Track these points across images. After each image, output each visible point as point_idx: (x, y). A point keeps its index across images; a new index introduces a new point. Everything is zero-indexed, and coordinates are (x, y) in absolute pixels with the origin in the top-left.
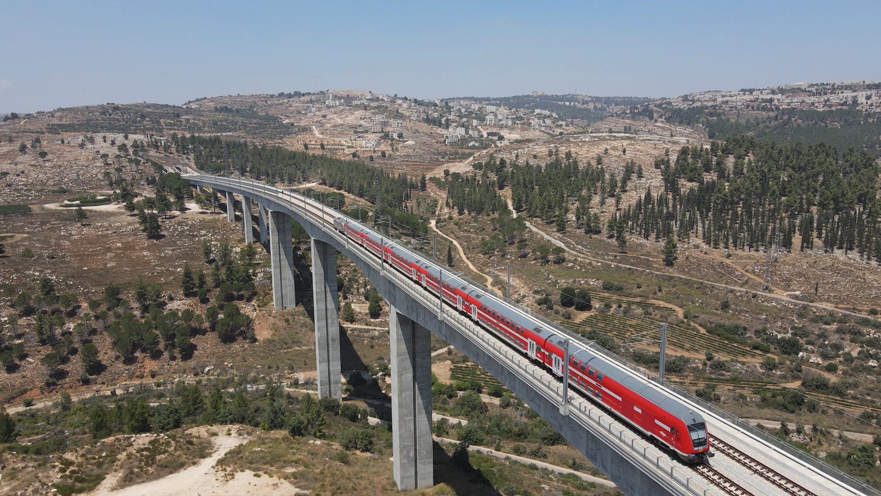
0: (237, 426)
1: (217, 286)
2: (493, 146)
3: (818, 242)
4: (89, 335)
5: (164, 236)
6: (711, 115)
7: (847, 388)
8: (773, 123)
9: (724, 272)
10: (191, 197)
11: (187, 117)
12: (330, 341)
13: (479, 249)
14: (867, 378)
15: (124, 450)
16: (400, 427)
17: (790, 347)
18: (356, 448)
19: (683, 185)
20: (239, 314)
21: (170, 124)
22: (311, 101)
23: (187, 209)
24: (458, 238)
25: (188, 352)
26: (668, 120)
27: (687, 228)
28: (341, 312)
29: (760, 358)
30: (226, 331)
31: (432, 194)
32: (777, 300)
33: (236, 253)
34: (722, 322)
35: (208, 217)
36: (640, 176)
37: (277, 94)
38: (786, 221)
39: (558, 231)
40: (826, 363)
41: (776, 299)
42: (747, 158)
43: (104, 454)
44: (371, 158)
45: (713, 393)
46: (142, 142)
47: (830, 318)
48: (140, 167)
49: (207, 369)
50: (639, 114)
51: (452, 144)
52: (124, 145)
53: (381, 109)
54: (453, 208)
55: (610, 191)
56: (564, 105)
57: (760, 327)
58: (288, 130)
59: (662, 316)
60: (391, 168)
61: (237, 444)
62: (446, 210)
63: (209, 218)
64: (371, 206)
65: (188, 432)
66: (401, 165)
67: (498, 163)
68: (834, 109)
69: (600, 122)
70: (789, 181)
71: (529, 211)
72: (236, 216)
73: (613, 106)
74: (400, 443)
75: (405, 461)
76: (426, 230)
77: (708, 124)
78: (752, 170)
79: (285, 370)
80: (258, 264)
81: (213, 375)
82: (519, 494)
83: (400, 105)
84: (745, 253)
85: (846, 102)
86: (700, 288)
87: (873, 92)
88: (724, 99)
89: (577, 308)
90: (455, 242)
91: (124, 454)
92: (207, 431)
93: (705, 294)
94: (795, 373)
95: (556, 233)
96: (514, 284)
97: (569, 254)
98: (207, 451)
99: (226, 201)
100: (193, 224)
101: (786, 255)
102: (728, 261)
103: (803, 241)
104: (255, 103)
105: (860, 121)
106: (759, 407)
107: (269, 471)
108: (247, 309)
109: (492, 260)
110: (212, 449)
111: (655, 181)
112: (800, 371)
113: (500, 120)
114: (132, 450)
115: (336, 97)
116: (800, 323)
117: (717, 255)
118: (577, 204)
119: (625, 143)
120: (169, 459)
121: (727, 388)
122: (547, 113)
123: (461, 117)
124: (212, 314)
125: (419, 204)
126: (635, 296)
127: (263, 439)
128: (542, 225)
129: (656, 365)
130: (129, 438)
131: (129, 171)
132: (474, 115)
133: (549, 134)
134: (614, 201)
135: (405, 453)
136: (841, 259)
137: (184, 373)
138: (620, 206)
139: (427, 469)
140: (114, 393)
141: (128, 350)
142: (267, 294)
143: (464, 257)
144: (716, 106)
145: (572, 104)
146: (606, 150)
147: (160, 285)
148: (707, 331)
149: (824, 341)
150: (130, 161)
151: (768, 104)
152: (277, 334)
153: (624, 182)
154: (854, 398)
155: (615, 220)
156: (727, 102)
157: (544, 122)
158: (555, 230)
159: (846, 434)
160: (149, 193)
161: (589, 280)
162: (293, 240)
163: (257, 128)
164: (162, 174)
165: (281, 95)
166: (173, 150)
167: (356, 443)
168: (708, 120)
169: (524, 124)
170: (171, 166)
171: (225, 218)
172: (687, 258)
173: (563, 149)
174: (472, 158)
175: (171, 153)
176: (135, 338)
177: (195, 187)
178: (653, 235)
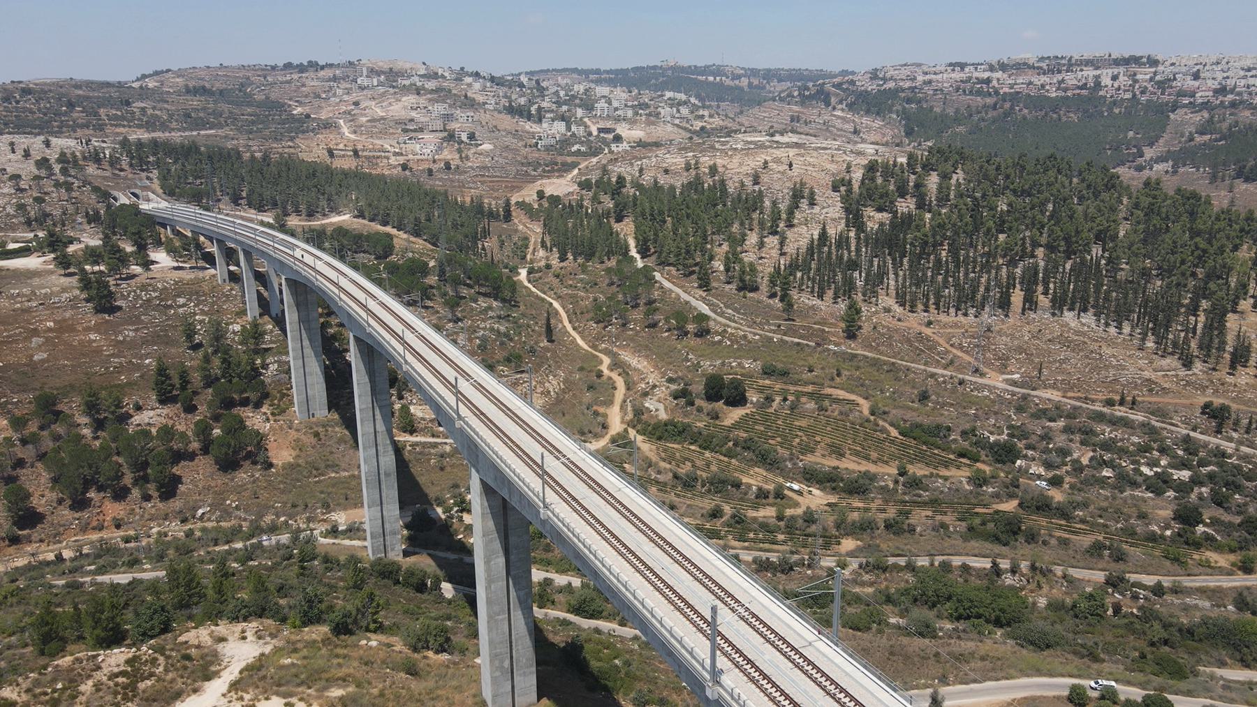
0: (254, 624)
1: (208, 385)
2: (606, 151)
3: (1044, 301)
4: (14, 468)
5: (120, 308)
6: (909, 101)
7: (1074, 508)
8: (992, 114)
9: (922, 347)
10: (158, 243)
11: (143, 105)
12: (382, 476)
13: (592, 314)
14: (1100, 494)
15: (89, 677)
16: (490, 630)
17: (1004, 454)
18: (428, 648)
19: (869, 217)
20: (245, 427)
21: (116, 117)
22: (335, 79)
23: (153, 262)
24: (559, 297)
25: (169, 489)
26: (851, 107)
27: (875, 282)
28: (395, 420)
29: (967, 469)
30: (226, 454)
31: (521, 227)
32: (991, 388)
33: (234, 332)
34: (919, 420)
35: (187, 276)
36: (812, 204)
37: (281, 64)
38: (1004, 270)
39: (700, 287)
40: (1050, 475)
41: (989, 386)
42: (955, 177)
43: (60, 686)
44: (430, 172)
45: (907, 522)
46: (73, 154)
47: (1055, 412)
48: (74, 194)
49: (200, 512)
50: (811, 97)
51: (548, 148)
52: (47, 160)
53: (441, 94)
54: (551, 251)
55: (772, 227)
56: (707, 83)
57: (968, 426)
58: (301, 125)
59: (841, 413)
60: (459, 187)
61: (257, 654)
62: (541, 253)
63: (188, 277)
64: (432, 250)
65: (182, 639)
66: (474, 182)
67: (614, 180)
68: (1069, 94)
69: (757, 108)
70: (1008, 211)
71: (659, 257)
72: (231, 273)
73: (775, 83)
74: (490, 650)
75: (498, 674)
76: (514, 286)
77: (905, 115)
78: (961, 196)
79: (317, 508)
80: (267, 350)
81: (209, 520)
82: (654, 703)
83: (470, 85)
84: (951, 319)
85: (1086, 84)
86: (891, 370)
87: (1122, 69)
88: (928, 77)
89: (728, 403)
90: (556, 305)
91: (90, 683)
92: (211, 635)
93: (897, 379)
94: (1011, 489)
95: (697, 291)
96: (639, 366)
97: (716, 322)
98: (213, 668)
99: (214, 249)
100: (165, 288)
101: (1003, 320)
102: (928, 331)
103: (1026, 300)
104: (248, 78)
105: (1102, 112)
106: (965, 539)
107: (305, 696)
108: (256, 420)
109: (609, 332)
110: (220, 665)
111: (831, 211)
112: (1017, 487)
113: (616, 109)
114: (101, 676)
115: (373, 72)
116: (1018, 419)
117: (914, 322)
118: (725, 247)
119: (792, 152)
120: (158, 686)
121: (925, 513)
122: (682, 97)
123: (559, 103)
124: (203, 431)
125: (502, 243)
126: (806, 383)
127: (294, 643)
128: (678, 278)
129: (834, 485)
130: (95, 657)
131: (56, 203)
132: (577, 101)
133: (685, 129)
134: (776, 242)
135: (497, 663)
136: (1073, 325)
137: (165, 519)
138: (786, 249)
139: (528, 682)
140: (59, 558)
141: (75, 489)
142: (285, 395)
143: (569, 328)
144: (916, 87)
145: (718, 78)
146: (766, 162)
147: (121, 387)
148: (900, 433)
149: (1048, 443)
150: (57, 185)
151: (984, 86)
152: (303, 455)
153: (791, 213)
154: (1083, 521)
155: (779, 273)
156: (930, 82)
157: (678, 111)
158: (696, 285)
159: (1071, 571)
160: (90, 239)
161: (744, 361)
162: (320, 310)
163: (253, 123)
164: (109, 207)
165: (288, 66)
166: (125, 165)
167: (427, 642)
168: (904, 108)
169: (650, 115)
170: (122, 190)
171: (214, 276)
172: (875, 328)
173: (706, 161)
174: (576, 171)
175: (121, 170)
176: (86, 471)
177: (164, 225)
178: (830, 294)
